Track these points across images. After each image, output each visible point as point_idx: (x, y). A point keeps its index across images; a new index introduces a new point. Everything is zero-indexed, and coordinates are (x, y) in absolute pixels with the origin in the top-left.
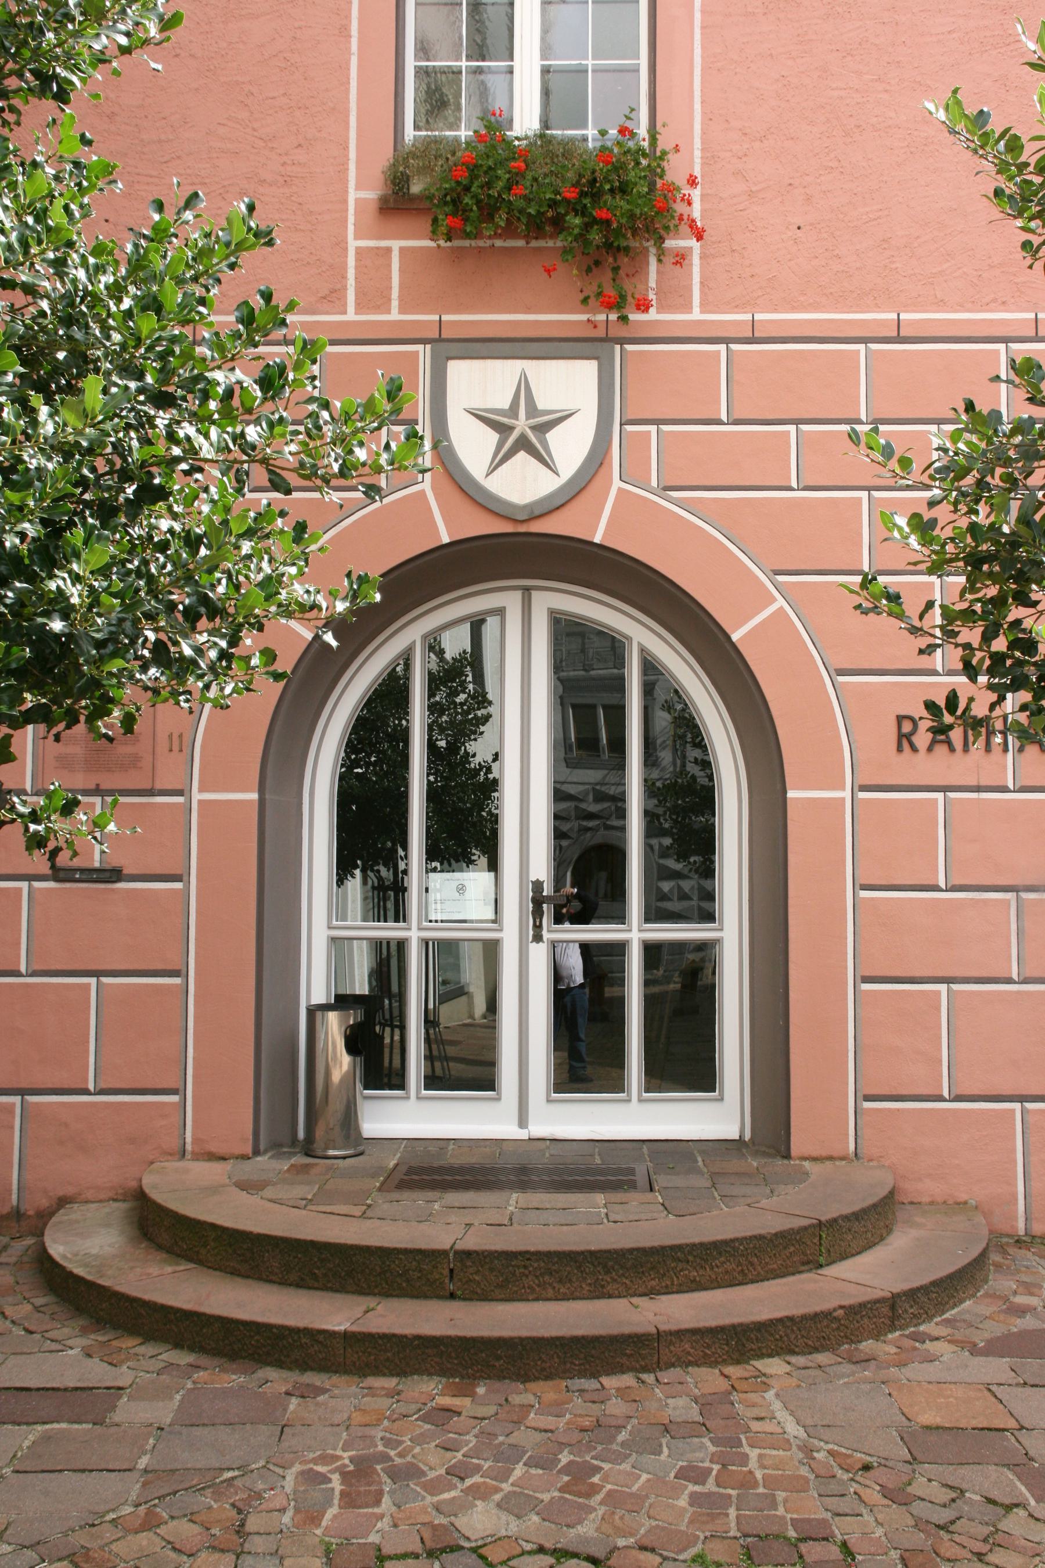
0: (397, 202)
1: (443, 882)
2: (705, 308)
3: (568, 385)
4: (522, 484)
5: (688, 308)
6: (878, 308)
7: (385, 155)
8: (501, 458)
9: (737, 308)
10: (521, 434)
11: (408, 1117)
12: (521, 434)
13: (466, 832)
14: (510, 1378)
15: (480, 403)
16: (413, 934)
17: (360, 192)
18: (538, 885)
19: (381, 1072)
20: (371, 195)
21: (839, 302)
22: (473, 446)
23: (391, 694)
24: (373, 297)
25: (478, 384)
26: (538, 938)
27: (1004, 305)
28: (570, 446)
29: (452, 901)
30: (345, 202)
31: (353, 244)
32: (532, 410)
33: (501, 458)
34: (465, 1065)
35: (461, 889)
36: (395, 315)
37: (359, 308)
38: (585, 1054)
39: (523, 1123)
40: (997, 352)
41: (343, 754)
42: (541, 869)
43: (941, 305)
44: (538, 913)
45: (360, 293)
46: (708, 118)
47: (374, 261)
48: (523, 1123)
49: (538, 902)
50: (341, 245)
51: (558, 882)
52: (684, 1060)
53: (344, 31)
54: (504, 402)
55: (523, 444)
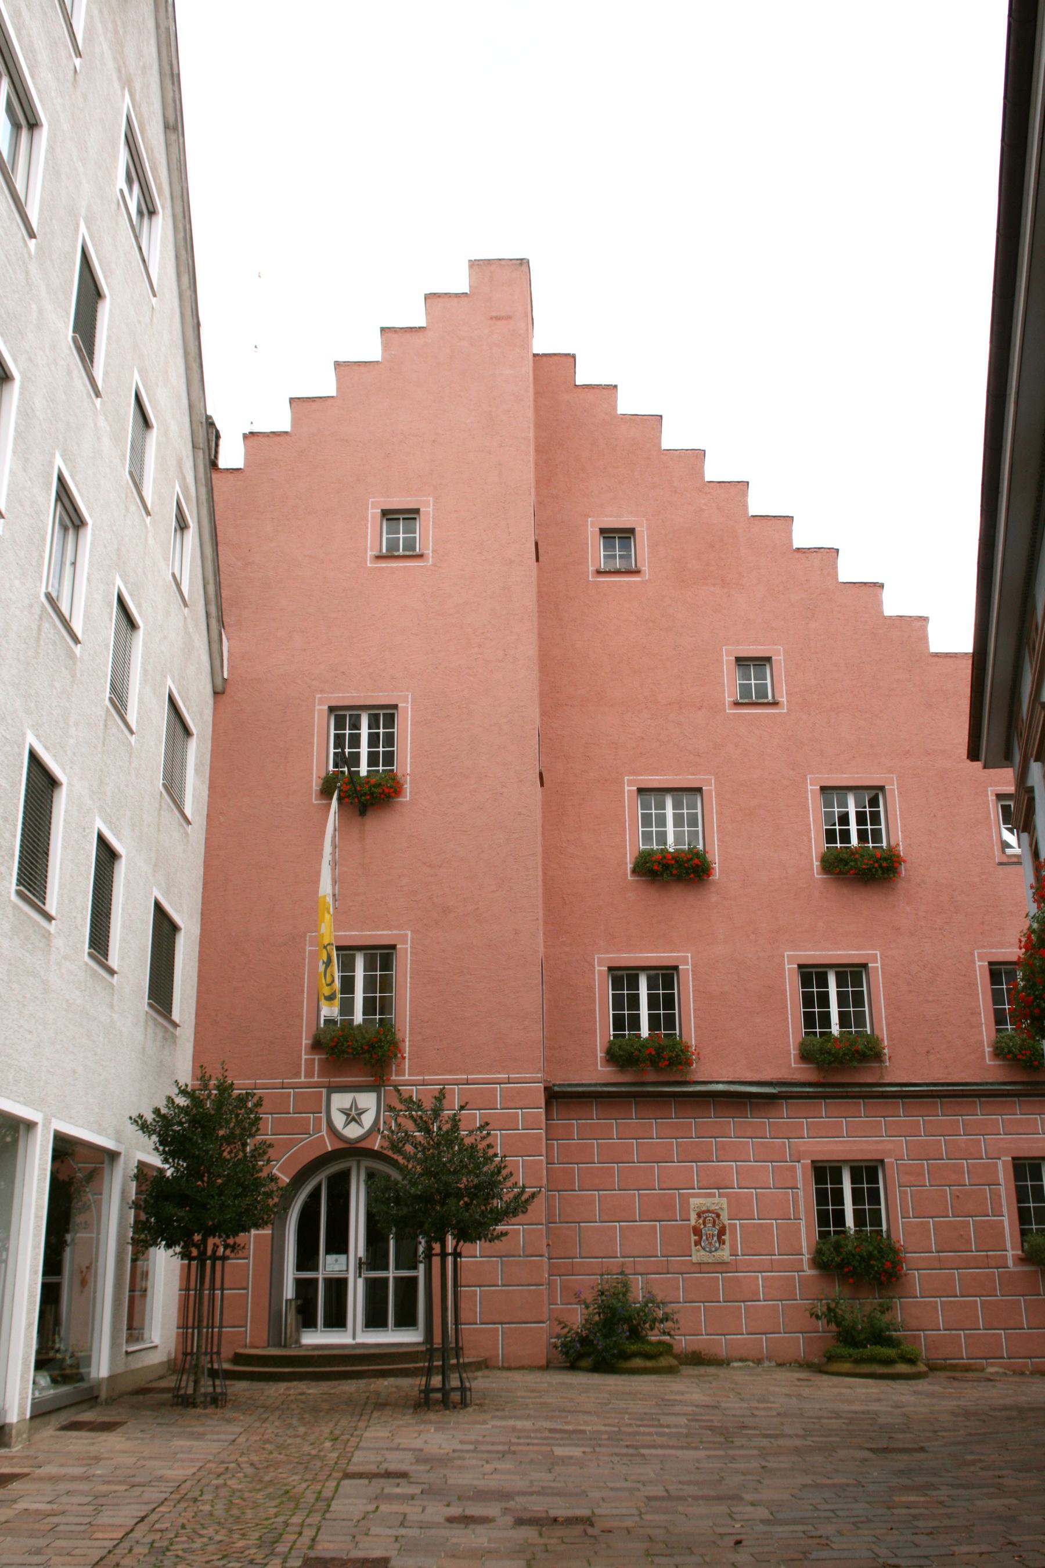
0: (317, 1045)
1: (331, 1258)
2: (409, 1075)
3: (368, 1101)
4: (353, 1132)
5: (404, 1075)
6: (461, 1074)
7: (313, 1031)
8: (346, 1124)
9: (419, 1075)
10: (353, 1116)
11: (316, 1338)
12: (353, 1116)
13: (339, 1244)
14: (390, 1030)
15: (340, 1107)
16: (320, 1276)
17: (306, 1042)
18: (360, 1259)
19: (308, 1322)
20: (309, 1042)
21: (450, 1072)
22: (339, 1120)
23: (315, 1195)
24: (309, 1074)
25: (341, 1101)
26: (360, 1276)
27: (499, 1073)
28: (368, 1119)
29: (330, 1265)
30: (301, 1044)
31: (304, 1057)
32: (357, 1109)
33: (346, 1124)
34: (337, 1319)
35: (336, 1261)
36: (316, 1079)
37: (306, 1077)
38: (375, 1319)
39: (354, 1338)
40: (731, 1167)
41: (198, 1410)
42: (361, 1253)
43: (480, 1073)
44: (360, 1268)
45: (306, 1072)
46: (411, 1016)
47: (310, 1063)
48: (354, 1338)
49: (360, 1264)
50: (300, 1058)
51: (367, 1258)
52: (405, 1319)
53: (303, 991)
54: (348, 1106)
55: (354, 1119)
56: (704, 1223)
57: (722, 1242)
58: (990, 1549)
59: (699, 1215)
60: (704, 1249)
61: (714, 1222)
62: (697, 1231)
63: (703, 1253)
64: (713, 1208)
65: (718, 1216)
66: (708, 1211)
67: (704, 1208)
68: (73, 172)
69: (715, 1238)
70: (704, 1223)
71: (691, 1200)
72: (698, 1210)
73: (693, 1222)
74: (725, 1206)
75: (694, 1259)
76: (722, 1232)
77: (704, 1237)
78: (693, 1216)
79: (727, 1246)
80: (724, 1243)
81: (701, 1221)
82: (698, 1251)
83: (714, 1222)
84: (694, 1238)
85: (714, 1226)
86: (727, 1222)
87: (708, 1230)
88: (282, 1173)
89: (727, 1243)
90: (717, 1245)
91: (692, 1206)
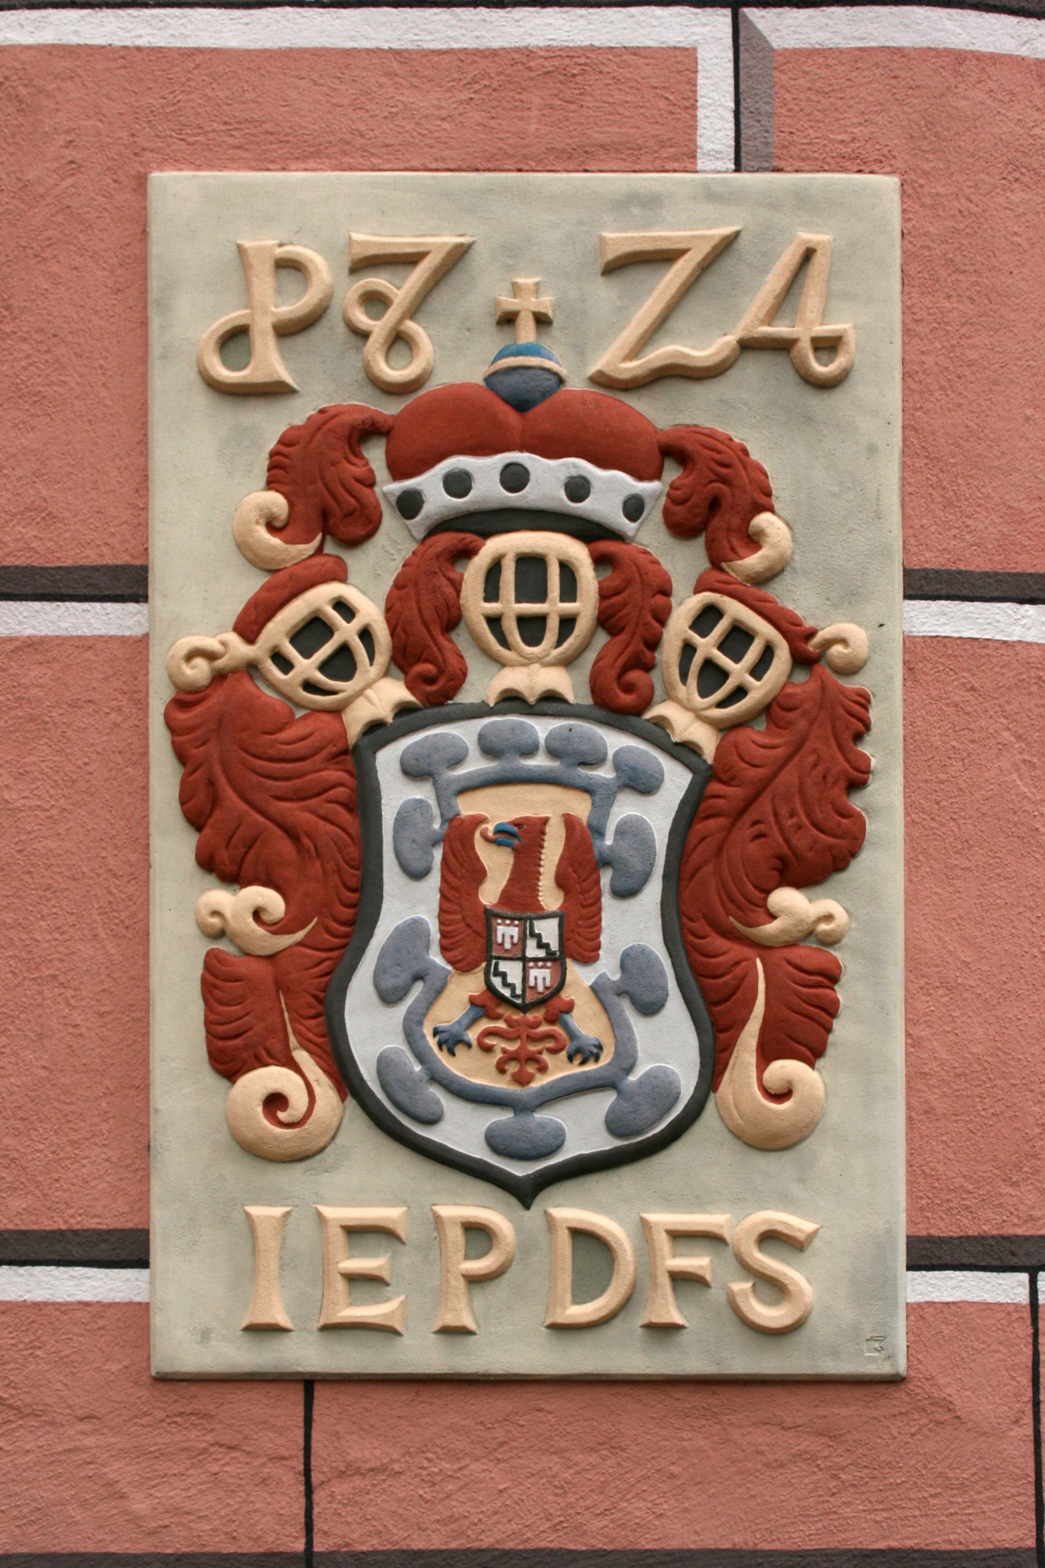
56: (425, 645)
57: (765, 1002)
58: (313, 444)
59: (323, 491)
60: (396, 1124)
61: (631, 613)
62: (271, 790)
63: (365, 1184)
64: (600, 345)
65: (717, 499)
66: (520, 411)
67: (452, 358)
68: (991, 1563)
69: (634, 924)
70: (425, 645)
71: (177, 190)
72: (322, 388)
73: (194, 613)
74: (866, 317)
75: (191, 1305)
76: (776, 807)
77: (408, 904)
78: (207, 504)
79: (859, 1090)
80: (803, 1028)
81: (364, 590)
82: (276, 1150)
83: (631, 613)
84: (193, 911)
85: (619, 700)
86: (877, 629)
87: (510, 761)
88: (518, 574)
89: (872, 1015)
90: (667, 1045)
91: (187, 324)
